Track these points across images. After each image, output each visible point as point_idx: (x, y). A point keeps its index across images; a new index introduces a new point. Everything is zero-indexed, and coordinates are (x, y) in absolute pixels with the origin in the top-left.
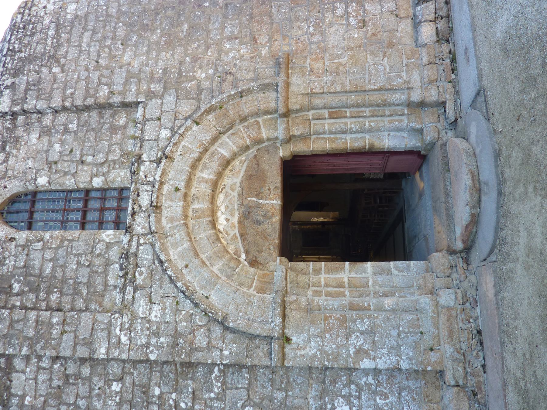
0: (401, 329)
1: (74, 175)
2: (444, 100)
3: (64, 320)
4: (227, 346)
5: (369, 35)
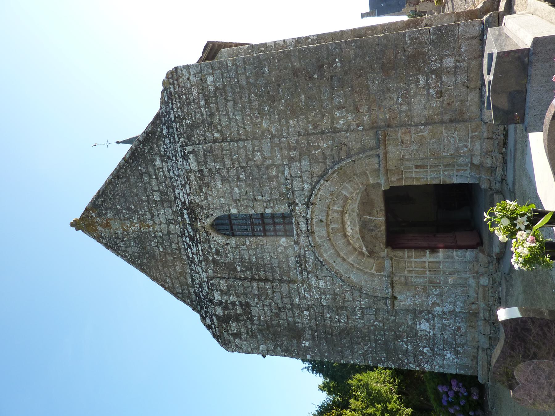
1: (253, 208)
5: (444, 105)
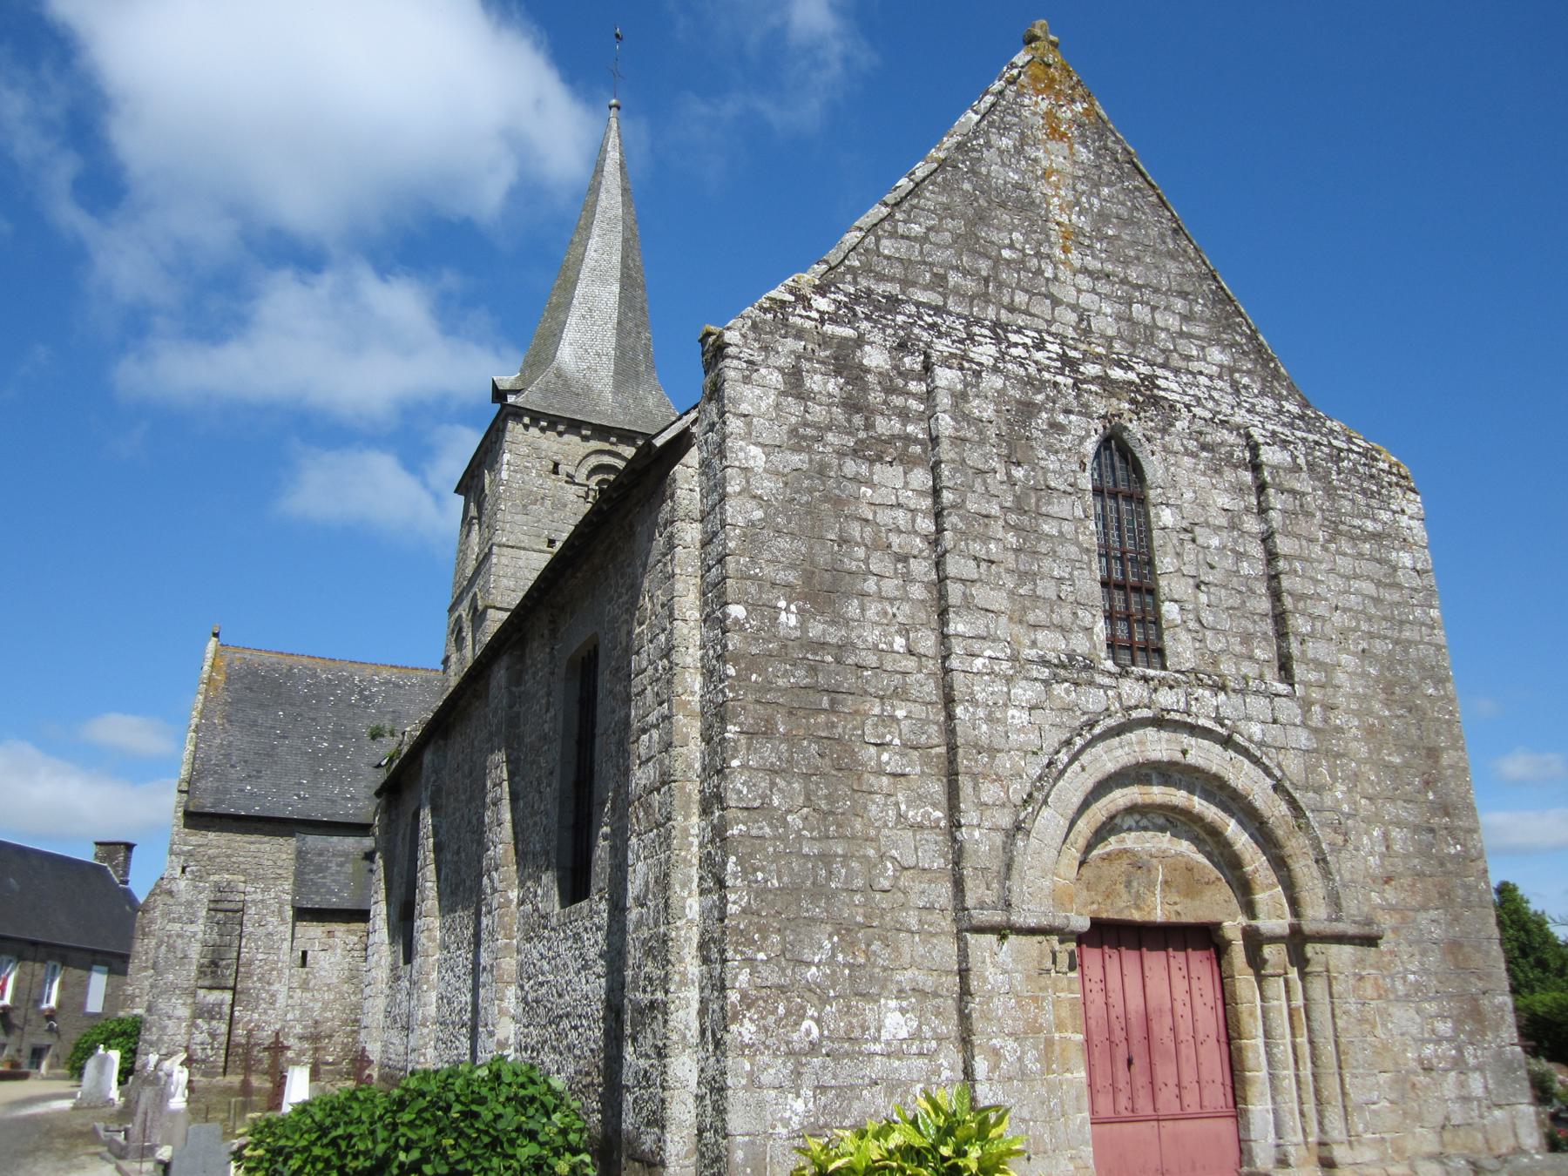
3: (993, 562)
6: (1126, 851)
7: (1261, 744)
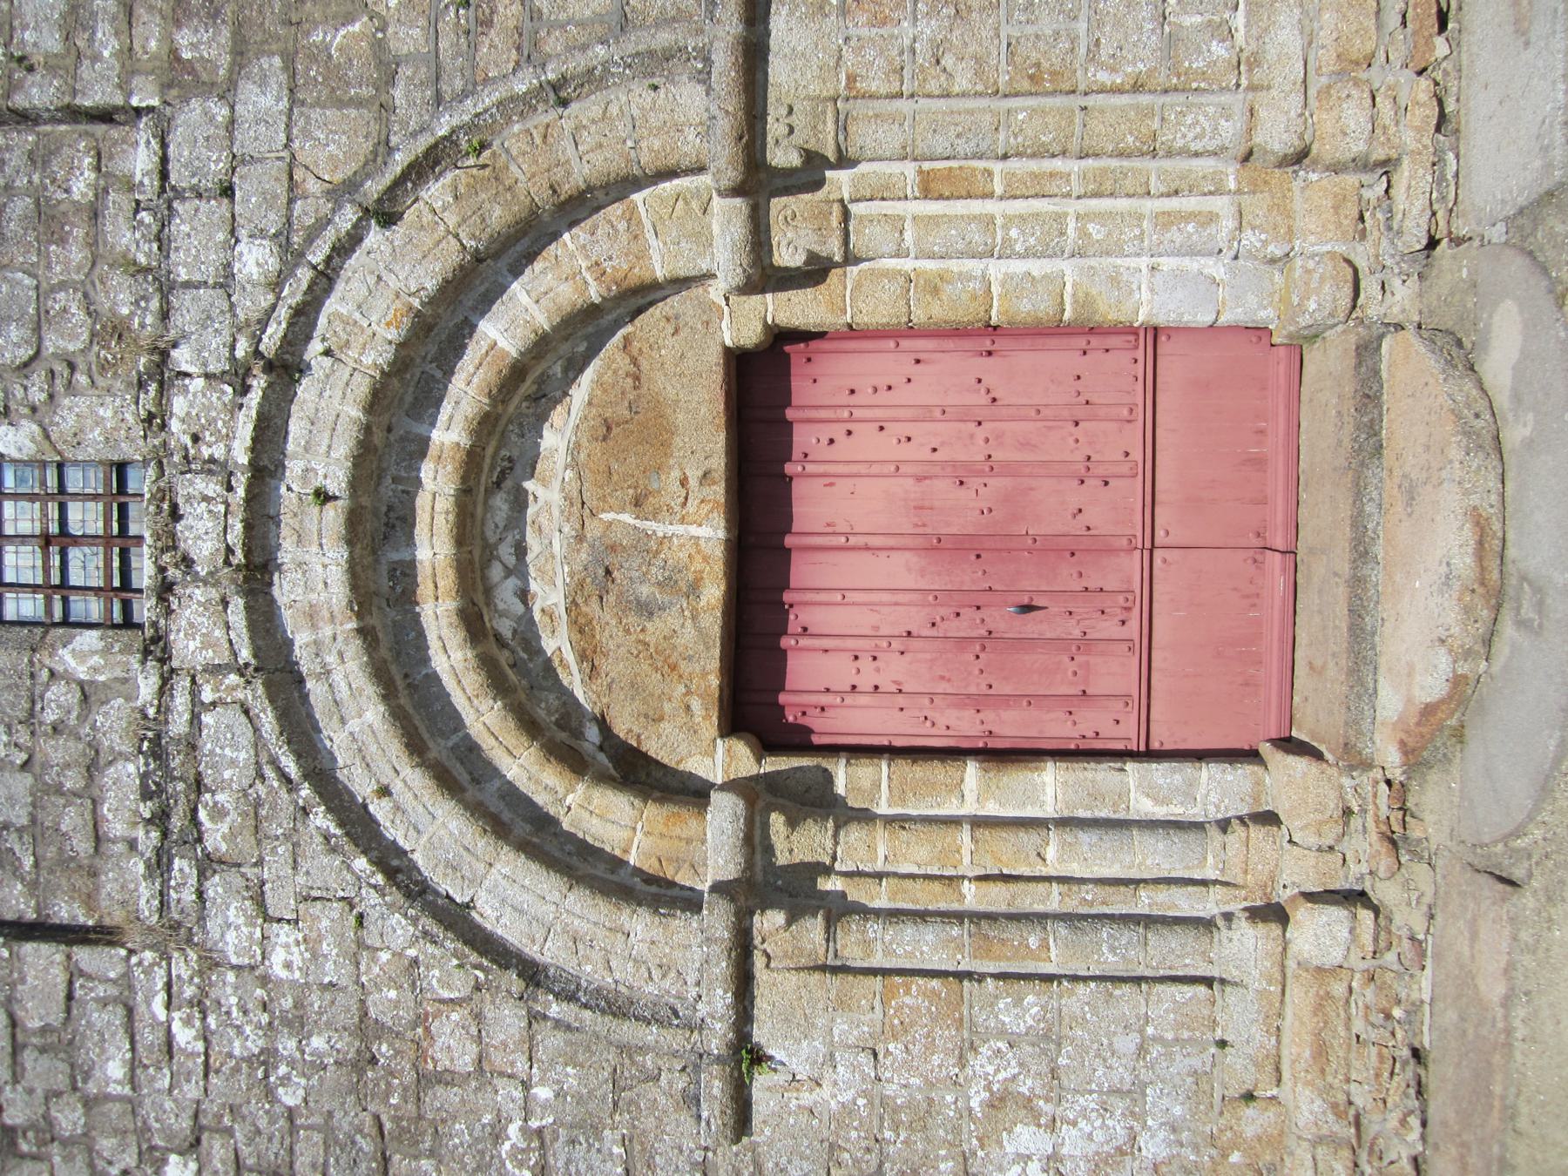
0: (1150, 1030)
2: (1393, 154)
4: (544, 1072)
6: (572, 606)
7: (291, 257)
